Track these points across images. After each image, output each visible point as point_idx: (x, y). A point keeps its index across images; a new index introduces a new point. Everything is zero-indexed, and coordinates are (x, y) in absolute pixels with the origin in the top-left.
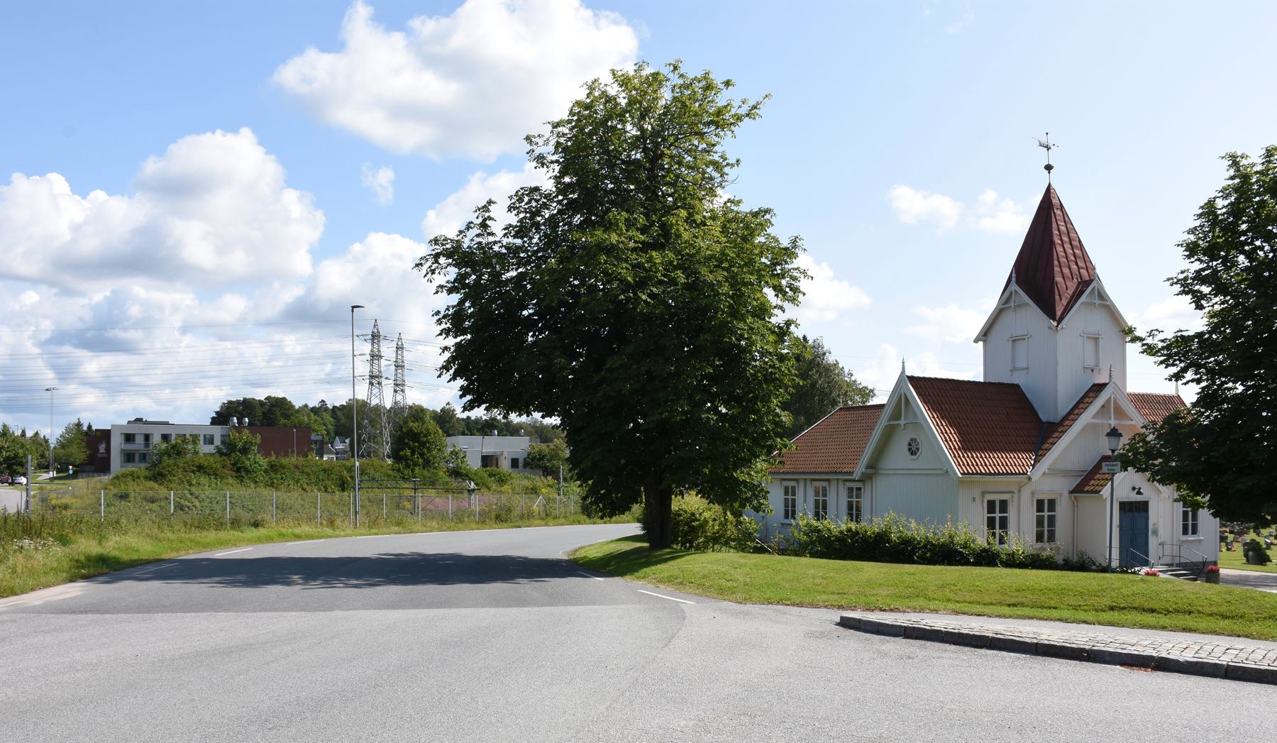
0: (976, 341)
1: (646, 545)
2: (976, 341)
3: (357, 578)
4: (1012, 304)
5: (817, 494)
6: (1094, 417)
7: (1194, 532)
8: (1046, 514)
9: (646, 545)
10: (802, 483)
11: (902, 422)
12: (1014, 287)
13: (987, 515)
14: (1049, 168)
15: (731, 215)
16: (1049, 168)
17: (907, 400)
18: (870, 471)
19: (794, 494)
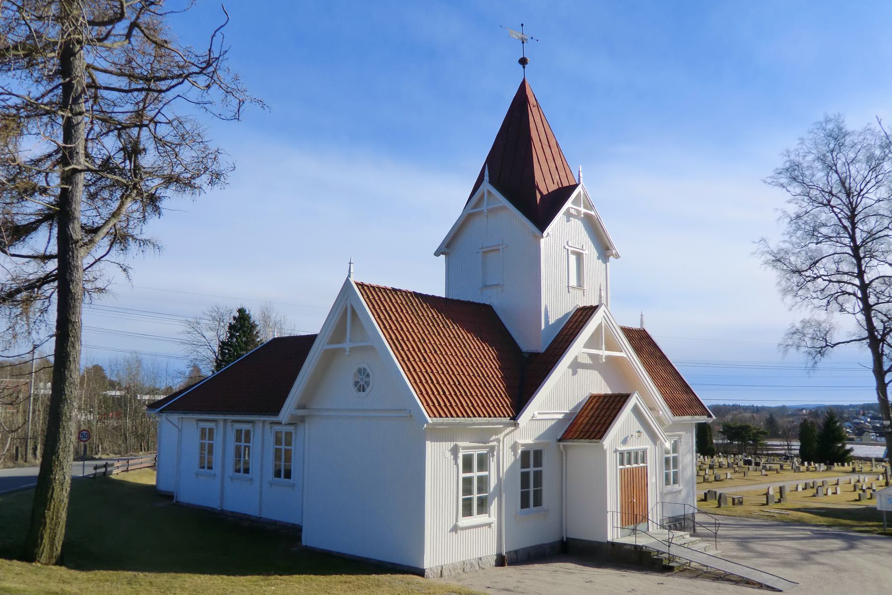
0: (437, 254)
1: (543, 327)
2: (437, 254)
3: (48, 492)
4: (484, 207)
5: (278, 441)
6: (586, 346)
7: (675, 482)
8: (532, 469)
9: (543, 327)
10: (221, 424)
11: (347, 345)
12: (486, 186)
13: (874, 456)
14: (523, 62)
15: (45, 119)
16: (523, 62)
17: (354, 312)
18: (301, 412)
19: (211, 438)
